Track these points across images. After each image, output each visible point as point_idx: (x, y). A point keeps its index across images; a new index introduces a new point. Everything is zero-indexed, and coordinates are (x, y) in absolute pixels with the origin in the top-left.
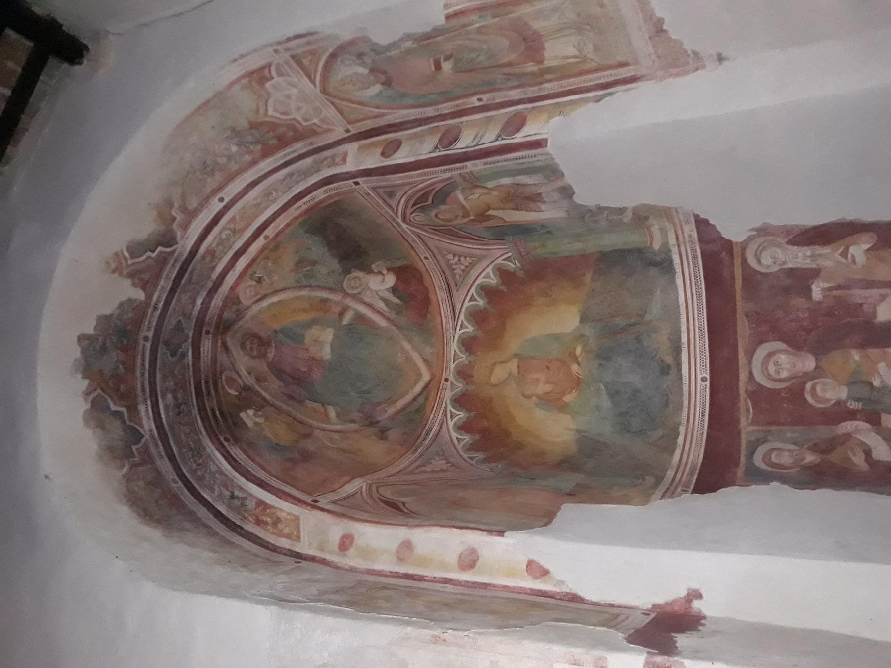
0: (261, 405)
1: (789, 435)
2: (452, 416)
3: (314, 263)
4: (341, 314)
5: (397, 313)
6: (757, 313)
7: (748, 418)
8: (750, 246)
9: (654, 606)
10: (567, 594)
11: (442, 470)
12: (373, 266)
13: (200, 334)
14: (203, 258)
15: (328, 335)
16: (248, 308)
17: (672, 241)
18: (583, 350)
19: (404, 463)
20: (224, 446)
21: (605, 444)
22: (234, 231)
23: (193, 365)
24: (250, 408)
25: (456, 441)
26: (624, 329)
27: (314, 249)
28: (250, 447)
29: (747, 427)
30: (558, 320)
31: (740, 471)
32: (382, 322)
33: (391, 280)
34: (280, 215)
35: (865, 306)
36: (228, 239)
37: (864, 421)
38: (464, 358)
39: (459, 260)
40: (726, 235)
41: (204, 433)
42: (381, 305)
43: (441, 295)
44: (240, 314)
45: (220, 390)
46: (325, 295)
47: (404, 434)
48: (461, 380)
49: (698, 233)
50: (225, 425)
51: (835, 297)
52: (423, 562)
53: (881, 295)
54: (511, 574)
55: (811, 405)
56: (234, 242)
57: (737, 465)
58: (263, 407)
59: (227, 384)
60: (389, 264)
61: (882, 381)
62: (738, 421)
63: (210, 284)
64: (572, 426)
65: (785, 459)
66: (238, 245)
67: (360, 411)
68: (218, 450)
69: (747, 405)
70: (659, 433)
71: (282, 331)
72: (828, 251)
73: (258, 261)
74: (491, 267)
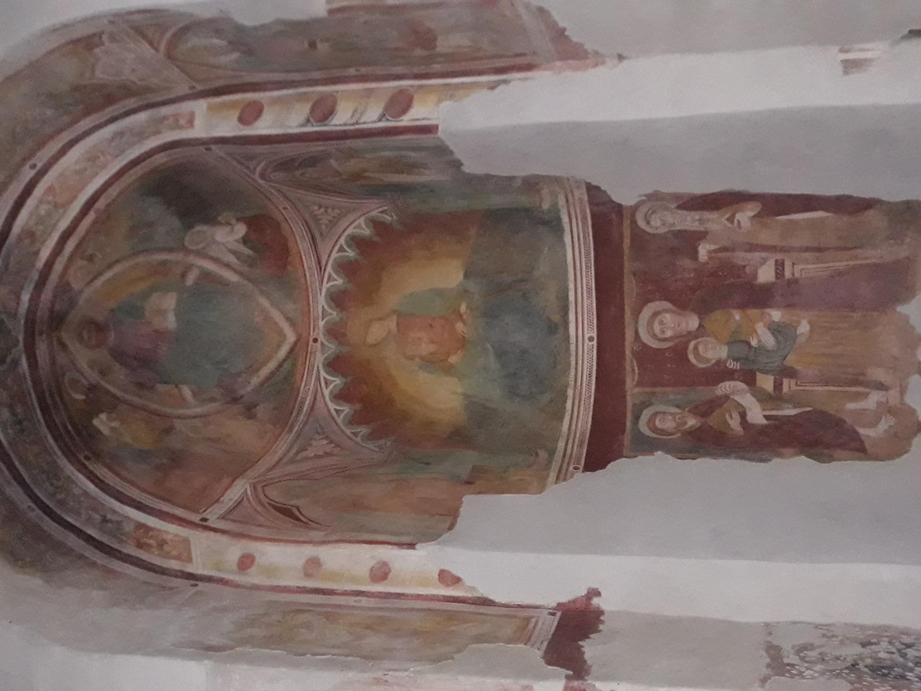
0: (112, 405)
1: (671, 397)
2: (326, 383)
3: (150, 225)
4: (184, 276)
7: (633, 380)
8: (640, 208)
9: (559, 605)
10: (479, 598)
11: (327, 454)
12: (219, 218)
13: (33, 334)
14: (20, 239)
15: (170, 301)
17: (561, 201)
19: (281, 447)
20: (86, 467)
22: (56, 206)
23: (31, 374)
24: (102, 412)
25: (334, 413)
28: (114, 463)
29: (632, 390)
30: (438, 276)
31: (627, 439)
32: (233, 278)
33: (241, 230)
35: (747, 268)
36: (49, 214)
38: (334, 314)
39: (326, 212)
40: (616, 198)
41: (59, 453)
42: (232, 259)
43: (302, 245)
44: (72, 304)
50: (81, 442)
52: (334, 576)
54: (424, 583)
55: (693, 365)
56: (58, 221)
57: (623, 431)
61: (759, 341)
62: (623, 383)
63: (35, 276)
65: (668, 424)
66: (64, 224)
68: (79, 471)
70: (547, 397)
72: (716, 216)
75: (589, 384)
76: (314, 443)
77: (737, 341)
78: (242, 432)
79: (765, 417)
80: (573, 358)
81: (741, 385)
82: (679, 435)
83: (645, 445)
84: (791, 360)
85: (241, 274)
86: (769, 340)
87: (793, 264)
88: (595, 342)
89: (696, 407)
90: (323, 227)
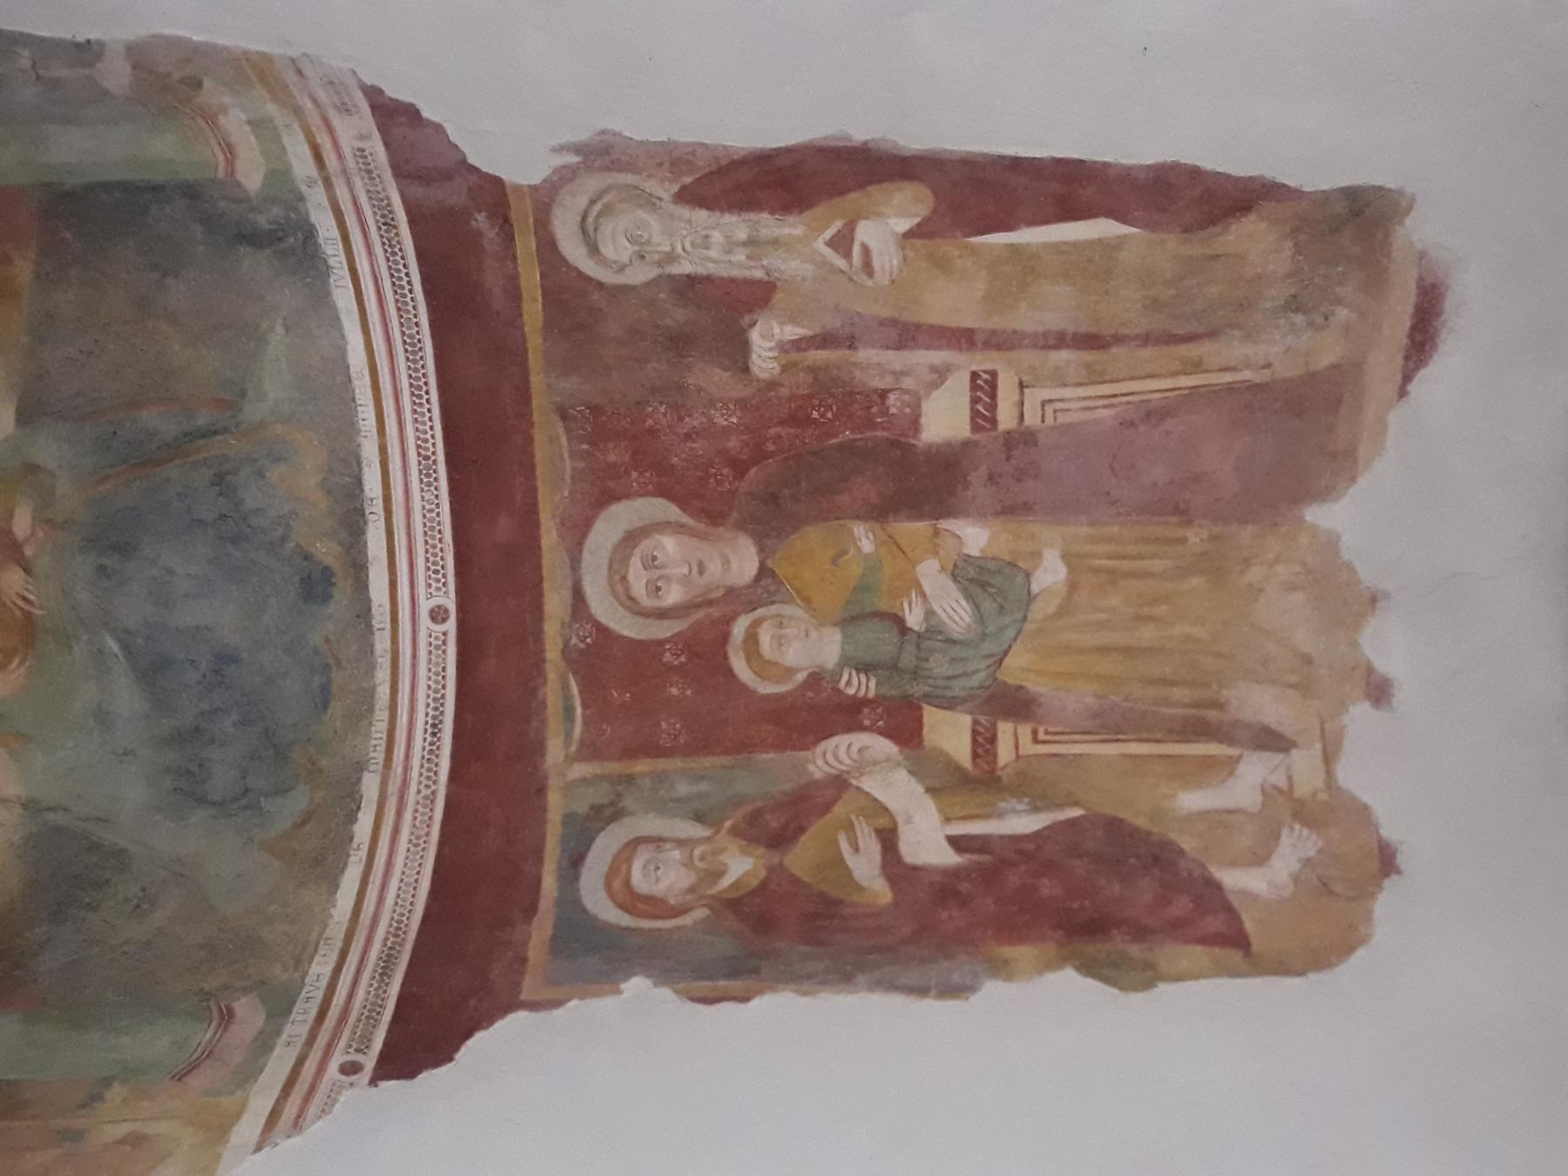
1: (683, 789)
6: (595, 410)
7: (568, 735)
17: (302, 166)
18: (43, 519)
29: (566, 767)
31: (541, 930)
35: (892, 397)
37: (881, 733)
49: (386, 145)
51: (813, 370)
53: (933, 369)
55: (744, 688)
57: (531, 910)
61: (930, 613)
62: (540, 748)
65: (665, 877)
69: (567, 698)
72: (799, 231)
75: (434, 750)
77: (866, 612)
79: (956, 842)
80: (382, 675)
81: (883, 746)
82: (700, 913)
83: (595, 956)
84: (1019, 668)
86: (956, 612)
87: (1022, 386)
88: (451, 625)
89: (755, 818)
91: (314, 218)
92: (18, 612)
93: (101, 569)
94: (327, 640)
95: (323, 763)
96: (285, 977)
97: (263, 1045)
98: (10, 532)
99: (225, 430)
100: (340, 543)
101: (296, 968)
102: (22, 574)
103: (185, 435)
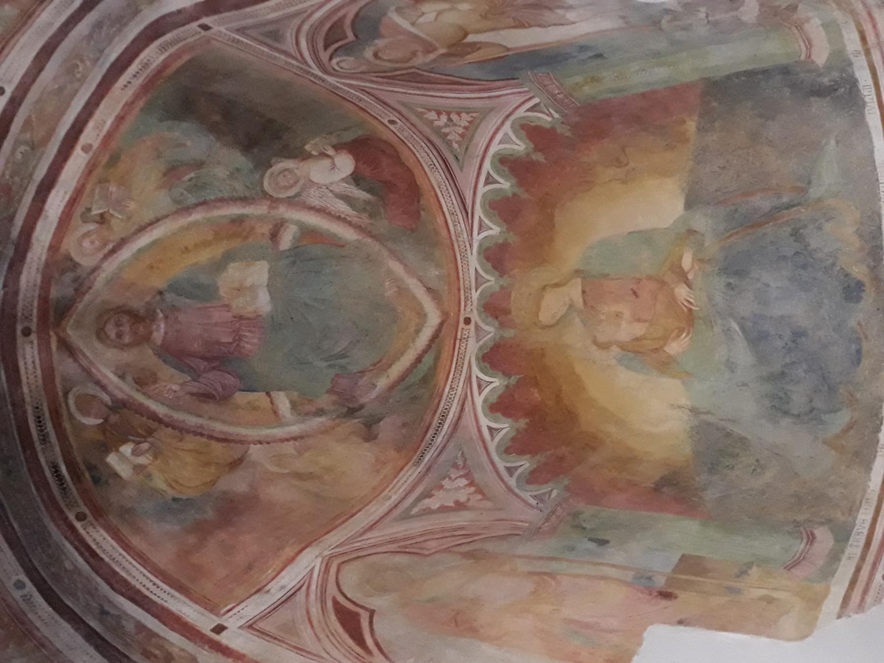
2: (479, 386)
3: (199, 165)
4: (274, 235)
5: (372, 216)
11: (460, 506)
12: (307, 147)
15: (258, 273)
16: (95, 269)
17: (852, 42)
18: (699, 260)
21: (742, 440)
24: (125, 441)
26: (771, 216)
27: (189, 143)
30: (642, 208)
32: (348, 234)
33: (346, 164)
34: (97, 105)
38: (492, 281)
39: (450, 120)
42: (342, 207)
43: (436, 178)
44: (81, 286)
45: (67, 425)
46: (235, 210)
47: (404, 425)
48: (490, 319)
56: (35, 168)
58: (150, 432)
59: (80, 409)
60: (334, 140)
64: (683, 401)
67: (331, 391)
70: (844, 417)
71: (175, 287)
73: (89, 187)
74: (508, 124)
76: (446, 483)
78: (351, 460)
85: (358, 228)
90: (456, 146)
91: (858, 75)
92: (685, 309)
93: (729, 285)
94: (859, 324)
95: (858, 396)
96: (843, 519)
97: (835, 557)
98: (681, 267)
99: (799, 204)
100: (868, 266)
101: (850, 514)
102: (688, 289)
103: (776, 208)
